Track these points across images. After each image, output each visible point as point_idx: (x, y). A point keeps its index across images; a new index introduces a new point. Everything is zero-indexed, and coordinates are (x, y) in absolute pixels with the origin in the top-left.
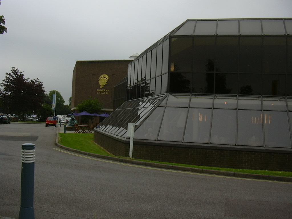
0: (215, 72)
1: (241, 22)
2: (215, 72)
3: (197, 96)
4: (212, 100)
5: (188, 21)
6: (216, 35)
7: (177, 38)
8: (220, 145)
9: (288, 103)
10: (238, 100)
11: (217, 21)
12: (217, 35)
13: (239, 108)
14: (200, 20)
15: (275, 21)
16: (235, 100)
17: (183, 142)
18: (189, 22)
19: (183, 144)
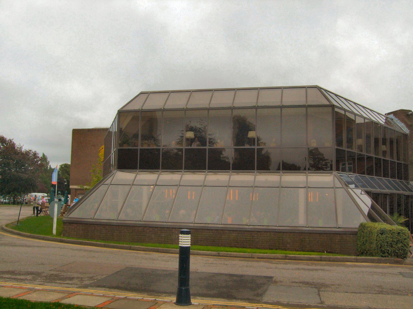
0: (207, 147)
1: (285, 90)
2: (207, 147)
3: (262, 174)
4: (279, 177)
5: (142, 93)
6: (232, 107)
7: (342, 107)
8: (255, 226)
9: (309, 177)
10: (281, 176)
11: (213, 91)
12: (164, 109)
13: (309, 185)
14: (278, 88)
15: (187, 92)
16: (305, 176)
17: (308, 227)
18: (142, 94)
19: (308, 229)
